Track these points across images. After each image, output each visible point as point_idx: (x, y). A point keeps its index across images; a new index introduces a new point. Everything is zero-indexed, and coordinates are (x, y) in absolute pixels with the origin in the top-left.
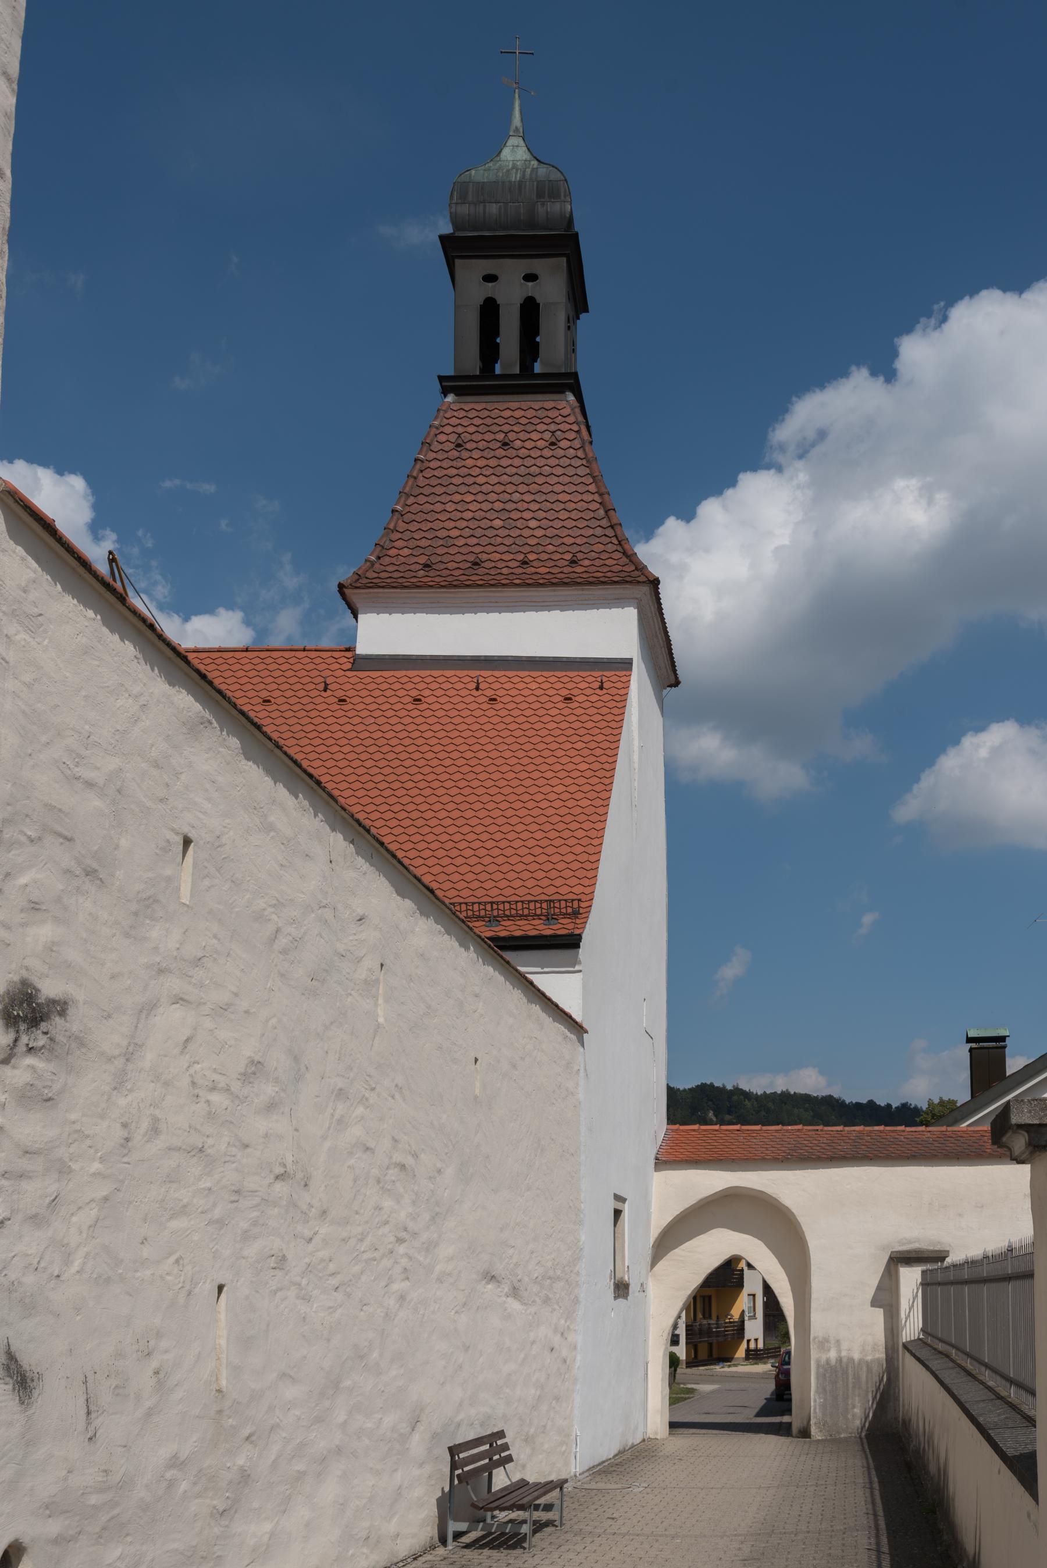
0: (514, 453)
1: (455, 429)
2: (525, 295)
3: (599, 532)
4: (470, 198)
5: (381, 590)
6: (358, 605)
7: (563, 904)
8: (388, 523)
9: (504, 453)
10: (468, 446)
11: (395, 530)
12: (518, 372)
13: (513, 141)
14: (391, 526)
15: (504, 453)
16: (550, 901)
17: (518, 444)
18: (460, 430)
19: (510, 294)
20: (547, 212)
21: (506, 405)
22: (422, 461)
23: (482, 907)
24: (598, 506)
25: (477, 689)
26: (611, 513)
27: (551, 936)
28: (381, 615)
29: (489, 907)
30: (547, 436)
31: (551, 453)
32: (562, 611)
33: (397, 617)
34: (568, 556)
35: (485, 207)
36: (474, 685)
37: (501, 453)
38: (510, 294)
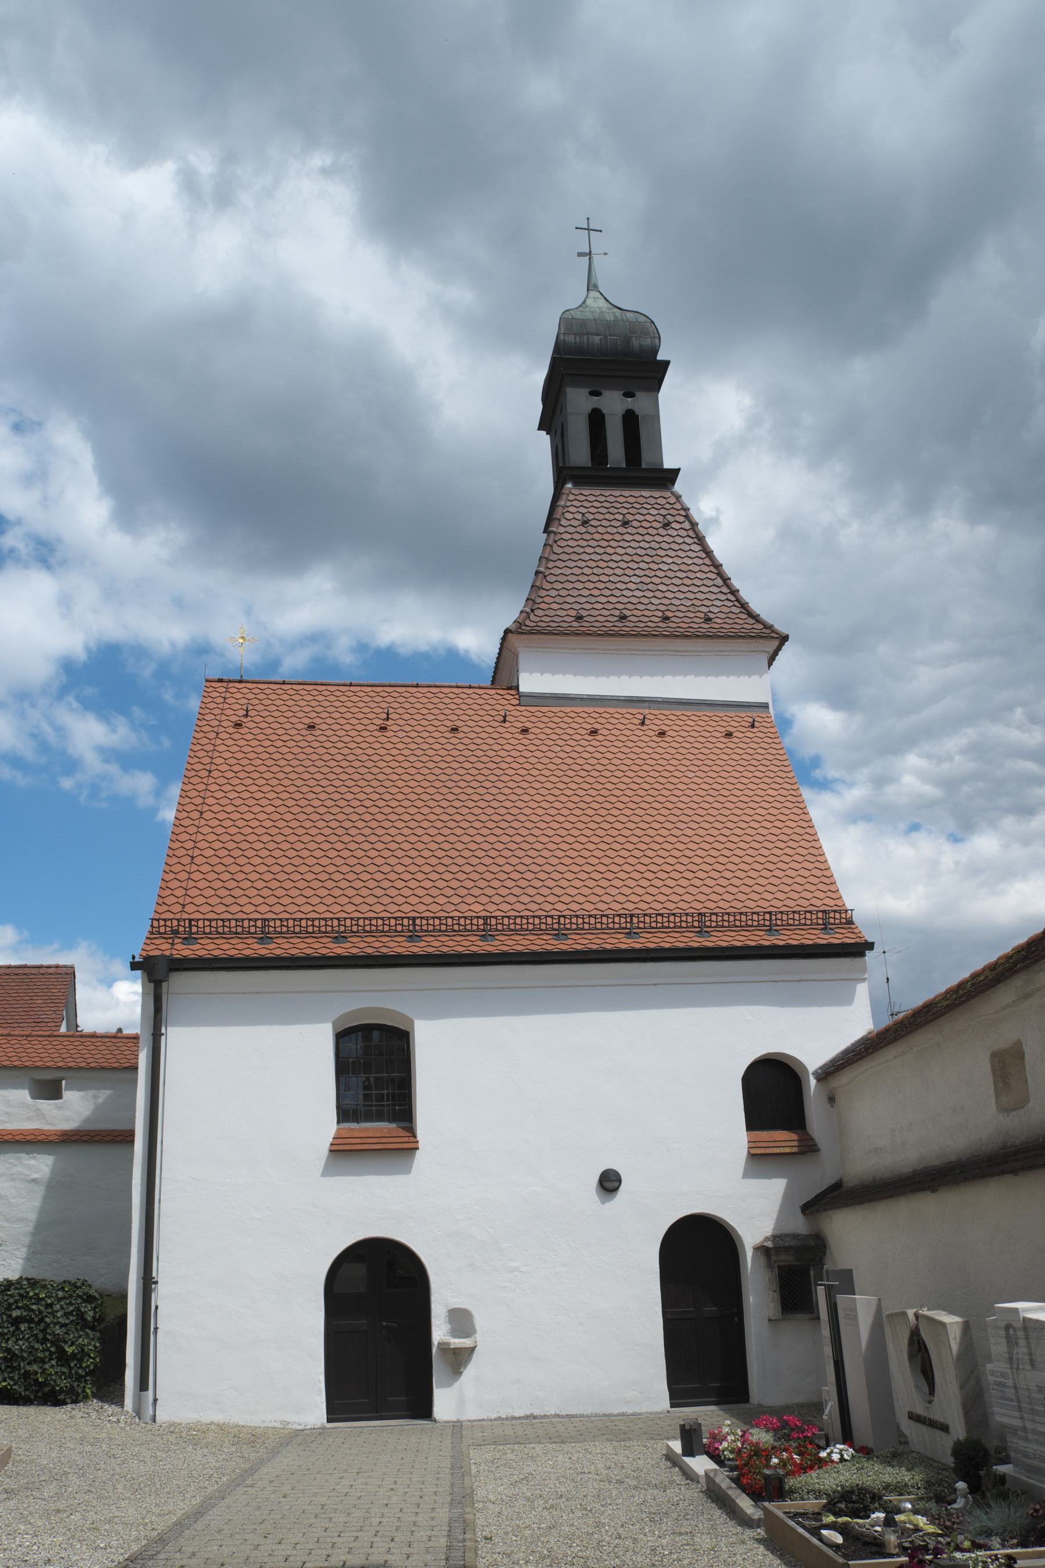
0: (592, 530)
7: (278, 923)
8: (535, 581)
9: (625, 530)
11: (540, 588)
14: (538, 584)
15: (625, 530)
16: (265, 920)
17: (635, 524)
18: (583, 510)
23: (354, 922)
24: (715, 576)
27: (727, 948)
30: (579, 516)
37: (622, 530)
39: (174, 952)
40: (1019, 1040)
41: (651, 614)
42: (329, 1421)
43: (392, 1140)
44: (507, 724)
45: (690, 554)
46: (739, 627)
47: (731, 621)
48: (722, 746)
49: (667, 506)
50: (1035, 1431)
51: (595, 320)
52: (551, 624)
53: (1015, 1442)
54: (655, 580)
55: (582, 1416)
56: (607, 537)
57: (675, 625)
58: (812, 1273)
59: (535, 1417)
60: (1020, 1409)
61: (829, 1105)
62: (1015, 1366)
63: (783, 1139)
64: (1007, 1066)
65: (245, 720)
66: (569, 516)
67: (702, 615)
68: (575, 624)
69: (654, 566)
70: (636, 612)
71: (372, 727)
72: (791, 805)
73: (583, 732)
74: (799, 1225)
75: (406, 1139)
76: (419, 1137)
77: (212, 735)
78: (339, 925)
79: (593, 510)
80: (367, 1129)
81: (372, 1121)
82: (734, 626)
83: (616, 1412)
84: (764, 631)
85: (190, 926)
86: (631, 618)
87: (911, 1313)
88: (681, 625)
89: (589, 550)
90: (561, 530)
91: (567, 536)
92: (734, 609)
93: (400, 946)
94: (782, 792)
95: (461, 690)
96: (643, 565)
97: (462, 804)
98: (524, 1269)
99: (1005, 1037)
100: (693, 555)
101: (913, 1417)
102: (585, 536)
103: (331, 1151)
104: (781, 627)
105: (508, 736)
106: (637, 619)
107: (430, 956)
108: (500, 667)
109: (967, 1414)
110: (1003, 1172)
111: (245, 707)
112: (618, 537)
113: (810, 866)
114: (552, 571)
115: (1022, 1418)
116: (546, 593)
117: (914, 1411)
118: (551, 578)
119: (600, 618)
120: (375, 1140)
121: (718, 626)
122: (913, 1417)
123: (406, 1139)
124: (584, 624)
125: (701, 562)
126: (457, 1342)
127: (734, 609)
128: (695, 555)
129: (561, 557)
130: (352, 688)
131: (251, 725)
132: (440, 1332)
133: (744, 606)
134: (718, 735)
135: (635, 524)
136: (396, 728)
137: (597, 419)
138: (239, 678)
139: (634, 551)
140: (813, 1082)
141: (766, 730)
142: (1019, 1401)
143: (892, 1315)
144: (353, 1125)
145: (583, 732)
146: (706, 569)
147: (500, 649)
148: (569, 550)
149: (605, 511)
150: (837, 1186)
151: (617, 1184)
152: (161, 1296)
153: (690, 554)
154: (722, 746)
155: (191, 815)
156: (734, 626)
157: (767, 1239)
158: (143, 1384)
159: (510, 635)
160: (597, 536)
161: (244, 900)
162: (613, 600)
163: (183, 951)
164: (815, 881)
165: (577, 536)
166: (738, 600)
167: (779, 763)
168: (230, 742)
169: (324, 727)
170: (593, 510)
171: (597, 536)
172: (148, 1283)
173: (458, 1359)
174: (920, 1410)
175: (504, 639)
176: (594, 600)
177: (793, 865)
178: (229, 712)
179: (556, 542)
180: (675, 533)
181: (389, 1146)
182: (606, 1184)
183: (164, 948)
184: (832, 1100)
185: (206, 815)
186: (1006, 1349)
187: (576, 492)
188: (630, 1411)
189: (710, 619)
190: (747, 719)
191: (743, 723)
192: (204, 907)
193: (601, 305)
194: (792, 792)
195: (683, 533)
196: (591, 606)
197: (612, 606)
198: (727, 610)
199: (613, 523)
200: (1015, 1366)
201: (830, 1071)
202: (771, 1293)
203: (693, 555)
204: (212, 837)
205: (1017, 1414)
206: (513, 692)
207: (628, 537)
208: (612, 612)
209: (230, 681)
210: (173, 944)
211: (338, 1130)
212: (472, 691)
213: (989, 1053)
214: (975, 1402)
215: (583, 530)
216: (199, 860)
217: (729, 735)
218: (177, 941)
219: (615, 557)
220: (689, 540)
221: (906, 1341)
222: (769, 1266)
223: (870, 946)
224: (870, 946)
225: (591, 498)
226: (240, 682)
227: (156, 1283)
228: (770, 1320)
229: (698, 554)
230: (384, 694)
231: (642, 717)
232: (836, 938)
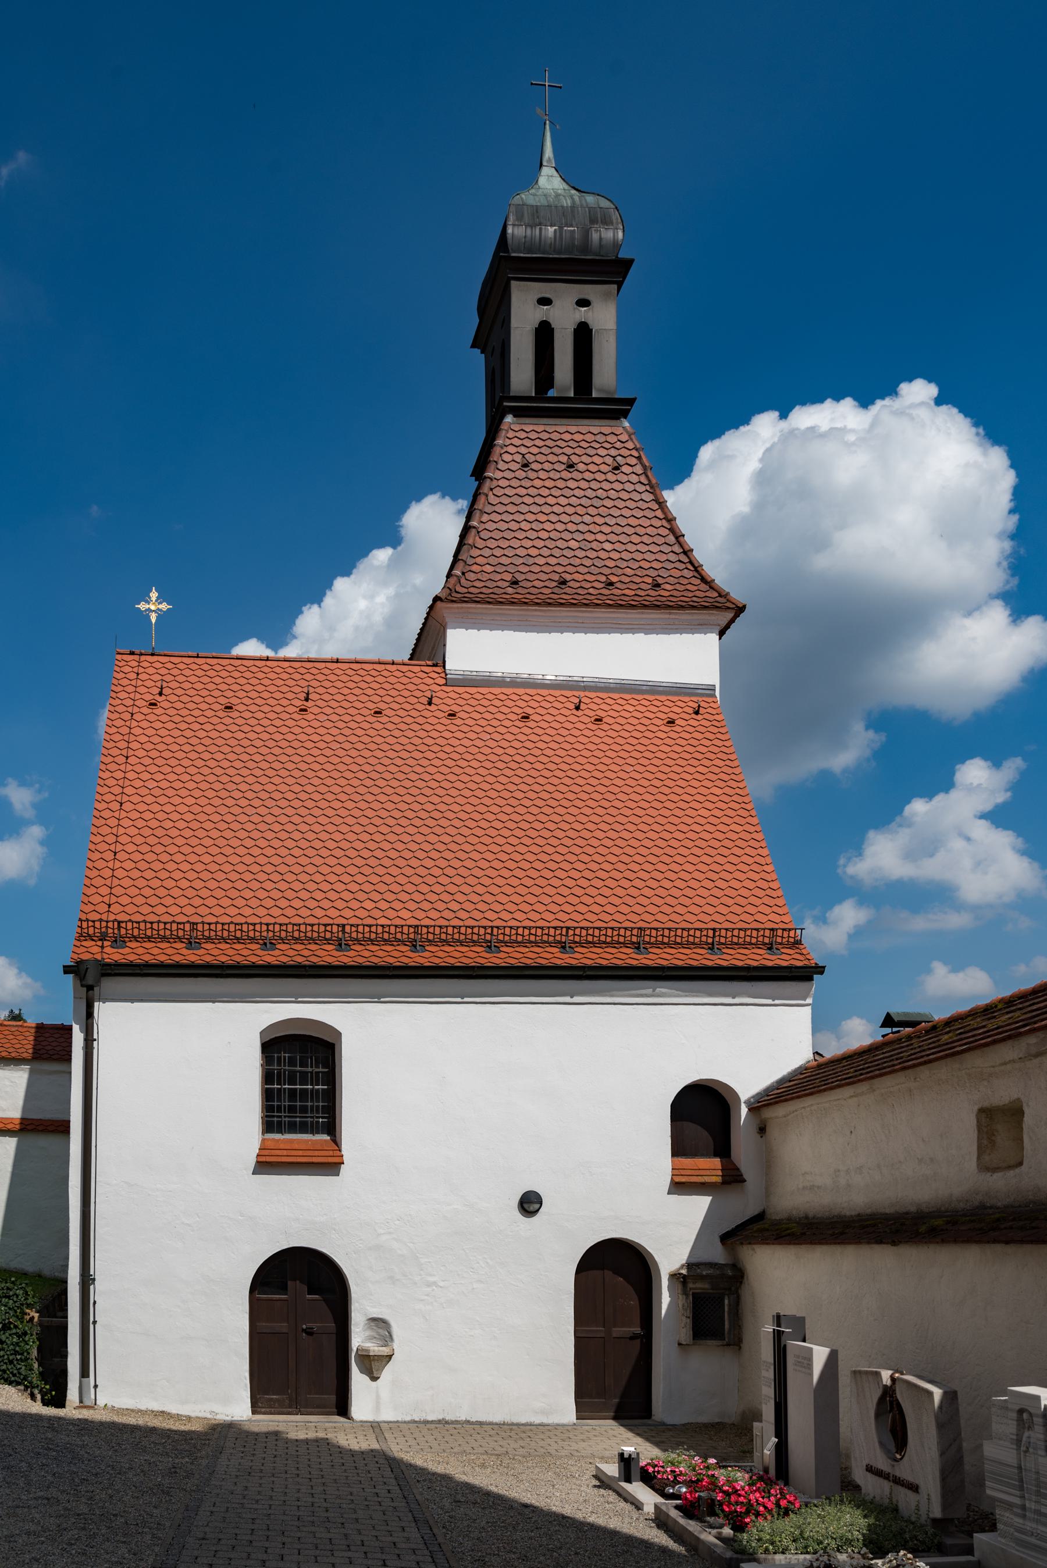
0: (532, 475)
1: (519, 449)
2: (578, 320)
3: (673, 557)
4: (526, 219)
5: (473, 605)
6: (447, 620)
9: (569, 475)
10: (534, 466)
12: (572, 395)
13: (547, 171)
15: (569, 475)
17: (581, 467)
18: (523, 450)
19: (564, 317)
20: (601, 239)
21: (553, 428)
22: (491, 480)
24: (667, 532)
25: (161, 694)
26: (681, 539)
27: (669, 968)
28: (708, 635)
29: (711, 933)
30: (518, 458)
31: (524, 475)
32: (646, 634)
33: (485, 633)
34: (508, 577)
35: (541, 229)
36: (158, 690)
37: (566, 475)
38: (564, 317)
39: (105, 956)
40: (1019, 1099)
41: (593, 578)
42: (253, 1413)
43: (316, 1153)
44: (433, 708)
45: (641, 504)
46: (690, 594)
47: (682, 588)
48: (663, 735)
49: (618, 445)
50: (1038, 1512)
51: (549, 206)
52: (484, 590)
53: (1003, 1515)
54: (601, 537)
55: (491, 1424)
56: (549, 483)
57: (619, 592)
58: (726, 1302)
59: (447, 1422)
60: (1021, 1488)
61: (758, 1136)
62: (1023, 1448)
63: (710, 1166)
64: (999, 1124)
65: (160, 699)
66: (507, 457)
67: (650, 580)
68: (510, 590)
69: (599, 520)
70: (576, 576)
71: (291, 709)
72: (736, 806)
73: (513, 717)
74: (717, 1254)
75: (331, 1153)
76: (344, 1152)
77: (127, 716)
78: (268, 930)
79: (535, 450)
80: (292, 1141)
81: (296, 1133)
82: (686, 594)
83: (523, 1422)
84: (719, 599)
85: (119, 927)
86: (571, 584)
87: (886, 1375)
88: (627, 592)
89: (528, 500)
90: (498, 475)
91: (503, 483)
92: (686, 573)
93: (328, 955)
94: (728, 790)
95: (383, 667)
96: (587, 519)
97: (281, 751)
98: (441, 1284)
99: (1002, 1093)
100: (644, 506)
101: (870, 1469)
102: (524, 483)
103: (257, 1162)
104: (738, 595)
105: (434, 721)
106: (578, 585)
107: (360, 967)
108: (423, 638)
109: (944, 1478)
110: (995, 1241)
111: (159, 684)
112: (561, 484)
113: (756, 877)
114: (487, 526)
115: (1023, 1497)
116: (478, 552)
117: (874, 1465)
118: (485, 535)
119: (537, 584)
120: (301, 1153)
121: (667, 594)
122: (870, 1469)
123: (331, 1153)
124: (520, 590)
125: (652, 514)
126: (374, 1348)
127: (686, 573)
128: (646, 505)
129: (496, 508)
130: (269, 663)
131: (166, 705)
132: (359, 1338)
133: (697, 568)
134: (659, 722)
135: (581, 467)
136: (316, 710)
137: (544, 334)
138: (150, 652)
139: (578, 501)
140: (744, 1110)
141: (711, 718)
142: (1021, 1481)
143: (860, 1372)
144: (278, 1136)
145: (513, 717)
146: (657, 523)
147: (426, 619)
148: (505, 500)
149: (549, 451)
150: (760, 1217)
151: (537, 1206)
152: (100, 1291)
153: (641, 504)
154: (663, 735)
155: (110, 806)
156: (686, 594)
157: (682, 1266)
158: (84, 1373)
159: (439, 604)
160: (538, 483)
161: (168, 901)
162: (553, 561)
163: (113, 955)
164: (761, 893)
165: (515, 483)
166: (691, 562)
167: (725, 757)
168: (145, 724)
169: (241, 708)
170: (535, 450)
171: (538, 483)
172: (87, 1280)
173: (372, 1365)
174: (882, 1463)
175: (431, 607)
176: (531, 561)
177: (737, 875)
178: (142, 690)
179: (491, 489)
180: (624, 478)
181: (315, 1160)
182: (526, 1206)
183: (92, 951)
184: (762, 1130)
185: (126, 806)
186: (1014, 1431)
187: (517, 428)
188: (537, 1422)
189: (658, 585)
190: (691, 704)
191: (687, 709)
192: (131, 906)
193: (556, 187)
194: (738, 791)
195: (634, 478)
196: (527, 569)
197: (551, 569)
198: (677, 574)
199: (556, 466)
200: (1023, 1448)
201: (763, 1102)
202: (684, 1318)
203: (644, 506)
204: (133, 831)
205: (1018, 1493)
206: (438, 669)
207: (572, 484)
208: (551, 576)
209: (141, 654)
210: (102, 947)
211: (263, 1140)
212: (394, 667)
213: (976, 1108)
214: (954, 1468)
215: (521, 474)
216: (121, 856)
217: (672, 722)
218: (106, 943)
219: (556, 509)
220: (640, 488)
221: (875, 1400)
222: (685, 1293)
223: (820, 970)
224: (820, 970)
225: (533, 435)
226: (153, 655)
227: (94, 1279)
228: (680, 1344)
229: (649, 505)
230: (303, 671)
231: (576, 701)
232: (784, 959)
